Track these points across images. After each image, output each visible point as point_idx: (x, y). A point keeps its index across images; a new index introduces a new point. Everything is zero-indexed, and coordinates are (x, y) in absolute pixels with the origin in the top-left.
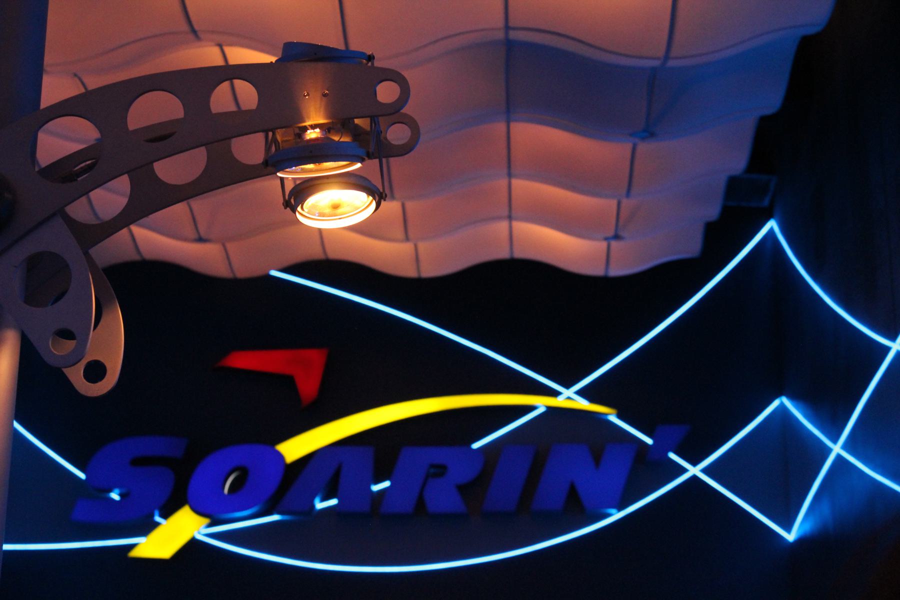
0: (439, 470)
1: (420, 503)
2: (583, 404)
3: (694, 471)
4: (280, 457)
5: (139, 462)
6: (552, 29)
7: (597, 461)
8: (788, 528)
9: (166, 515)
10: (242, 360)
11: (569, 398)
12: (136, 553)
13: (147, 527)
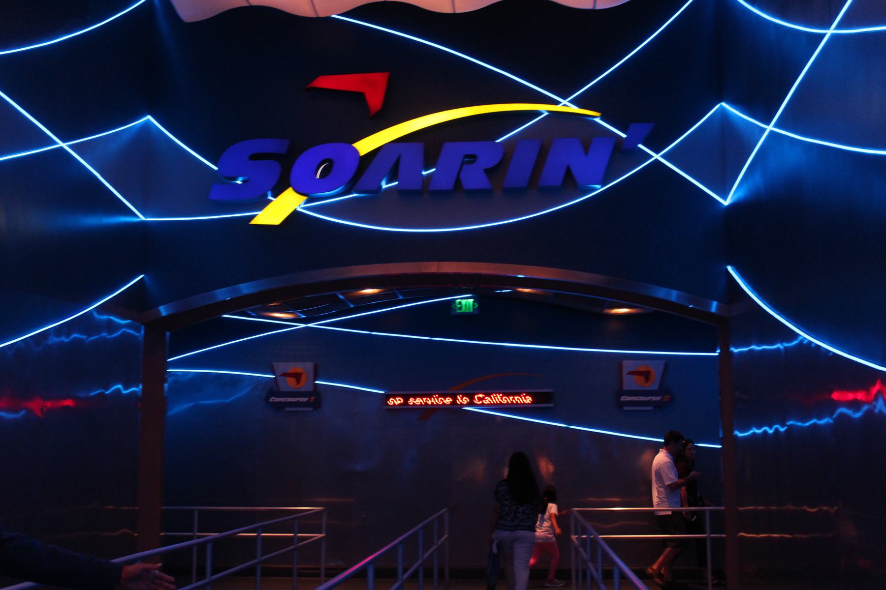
1: (458, 182)
2: (574, 109)
4: (356, 151)
5: (254, 157)
8: (725, 198)
9: (275, 196)
10: (326, 82)
11: (565, 105)
12: (255, 222)
13: (263, 204)
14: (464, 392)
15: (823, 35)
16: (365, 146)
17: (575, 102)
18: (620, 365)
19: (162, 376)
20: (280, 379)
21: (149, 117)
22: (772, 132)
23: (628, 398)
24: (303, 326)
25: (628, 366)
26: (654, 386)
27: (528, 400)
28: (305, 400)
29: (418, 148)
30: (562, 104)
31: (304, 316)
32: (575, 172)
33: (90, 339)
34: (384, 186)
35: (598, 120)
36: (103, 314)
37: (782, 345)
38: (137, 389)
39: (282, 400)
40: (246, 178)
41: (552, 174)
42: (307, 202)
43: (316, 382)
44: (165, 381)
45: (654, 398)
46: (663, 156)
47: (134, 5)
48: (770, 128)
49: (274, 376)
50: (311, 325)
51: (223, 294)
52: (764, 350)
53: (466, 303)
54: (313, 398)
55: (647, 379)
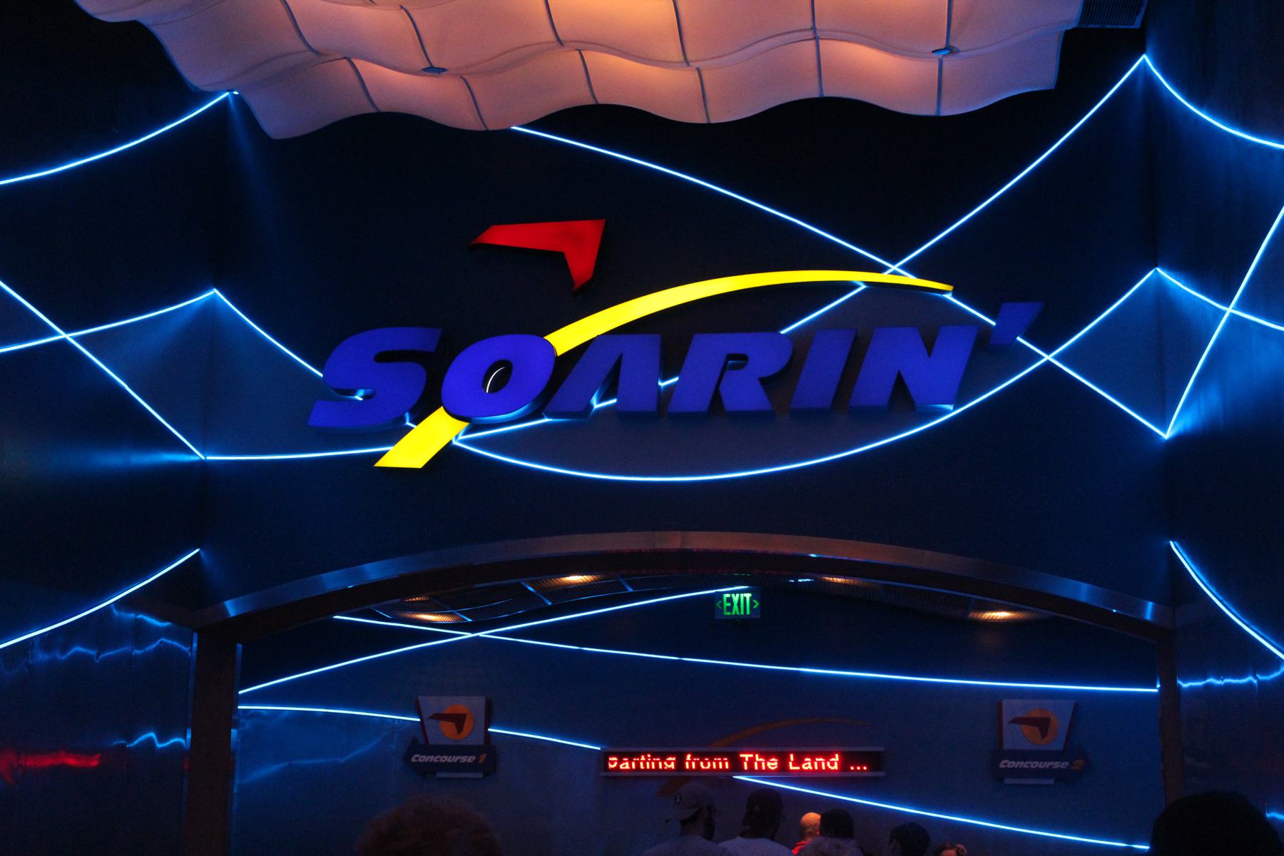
0: (740, 360)
1: (717, 398)
2: (910, 280)
4: (550, 347)
5: (383, 357)
7: (929, 347)
8: (1165, 430)
9: (417, 421)
10: (502, 236)
11: (894, 273)
12: (383, 463)
13: (395, 433)
14: (655, 749)
16: (565, 339)
17: (911, 268)
19: (228, 716)
20: (428, 723)
21: (215, 291)
22: (1232, 316)
23: (1013, 764)
24: (469, 635)
25: (1011, 709)
26: (1058, 746)
27: (834, 764)
28: (471, 759)
29: (650, 344)
30: (890, 271)
31: (470, 620)
32: (908, 380)
33: (102, 656)
34: (597, 406)
35: (949, 297)
36: (129, 611)
37: (1256, 678)
38: (181, 740)
39: (432, 759)
40: (369, 391)
42: (468, 432)
43: (490, 730)
44: (232, 724)
45: (1056, 765)
46: (1056, 358)
47: (1179, 101)
48: (1230, 310)
49: (419, 720)
50: (481, 634)
51: (333, 581)
52: (1228, 686)
53: (738, 599)
54: (483, 757)
55: (1044, 733)
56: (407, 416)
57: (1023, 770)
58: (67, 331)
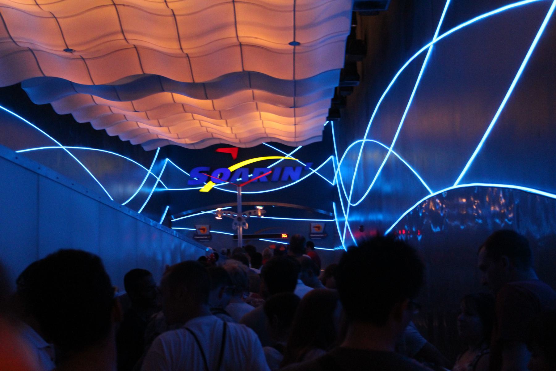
2: (293, 158)
3: (314, 171)
4: (229, 170)
5: (200, 172)
6: (119, 11)
11: (289, 157)
12: (201, 191)
13: (203, 185)
15: (362, 142)
16: (232, 169)
18: (310, 225)
25: (313, 225)
26: (321, 231)
29: (247, 170)
32: (292, 177)
41: (285, 177)
45: (322, 235)
55: (319, 229)
56: (432, 226)
57: (314, 236)
58: (63, 145)
